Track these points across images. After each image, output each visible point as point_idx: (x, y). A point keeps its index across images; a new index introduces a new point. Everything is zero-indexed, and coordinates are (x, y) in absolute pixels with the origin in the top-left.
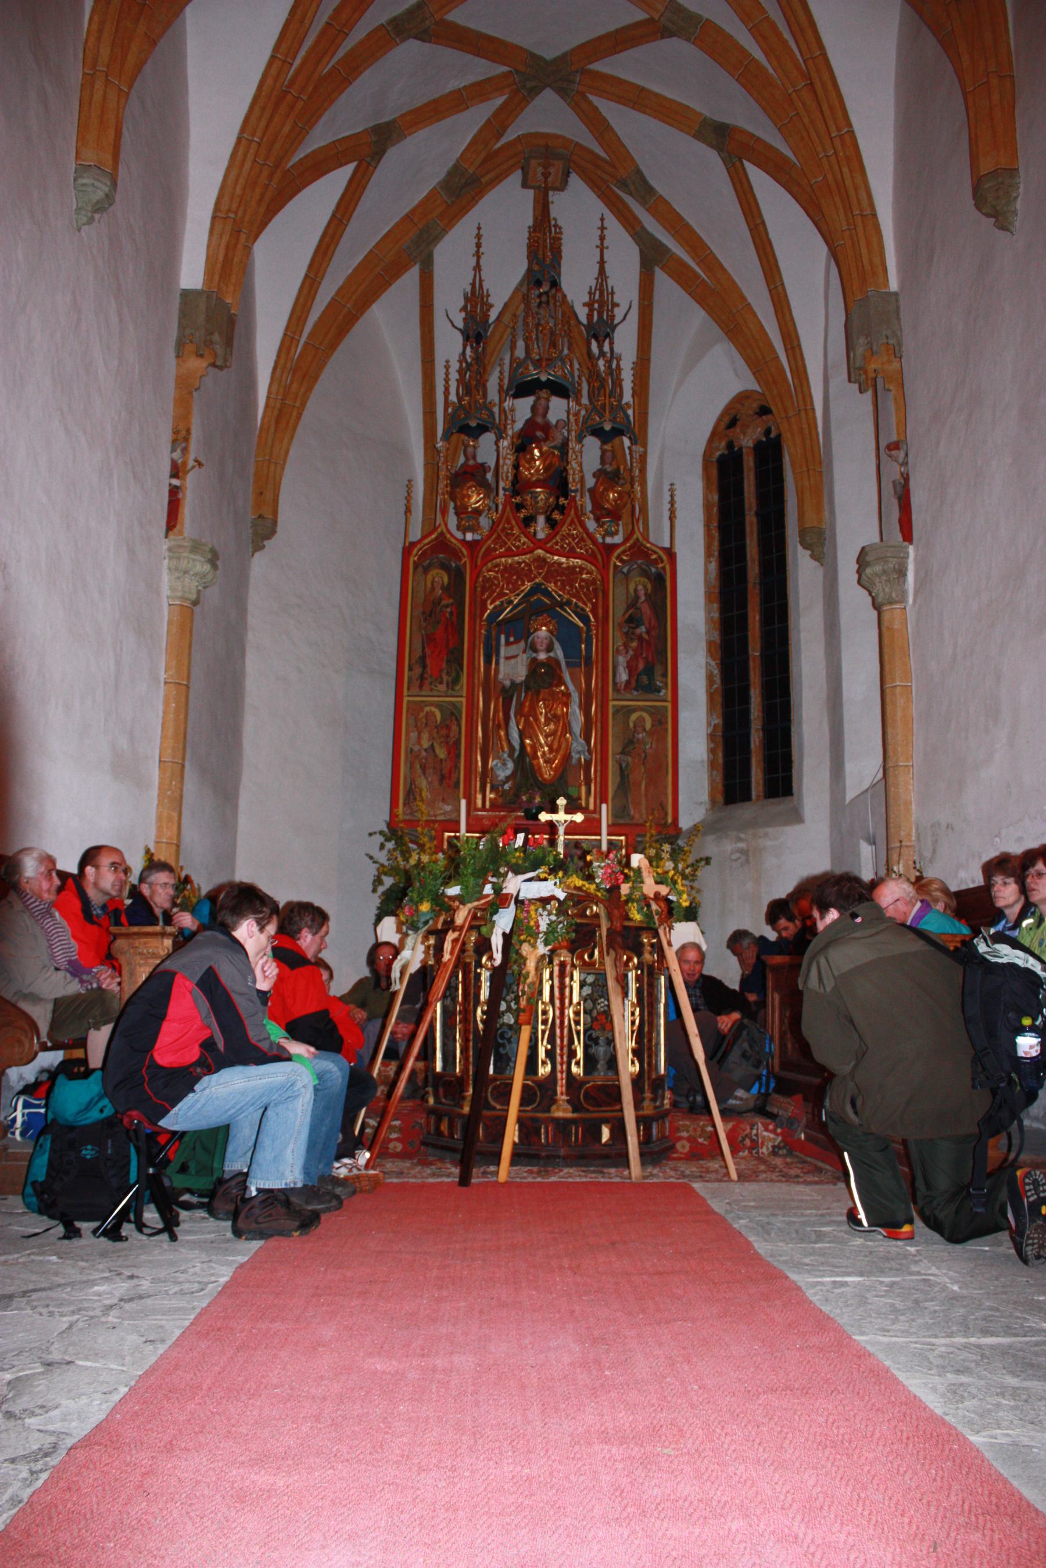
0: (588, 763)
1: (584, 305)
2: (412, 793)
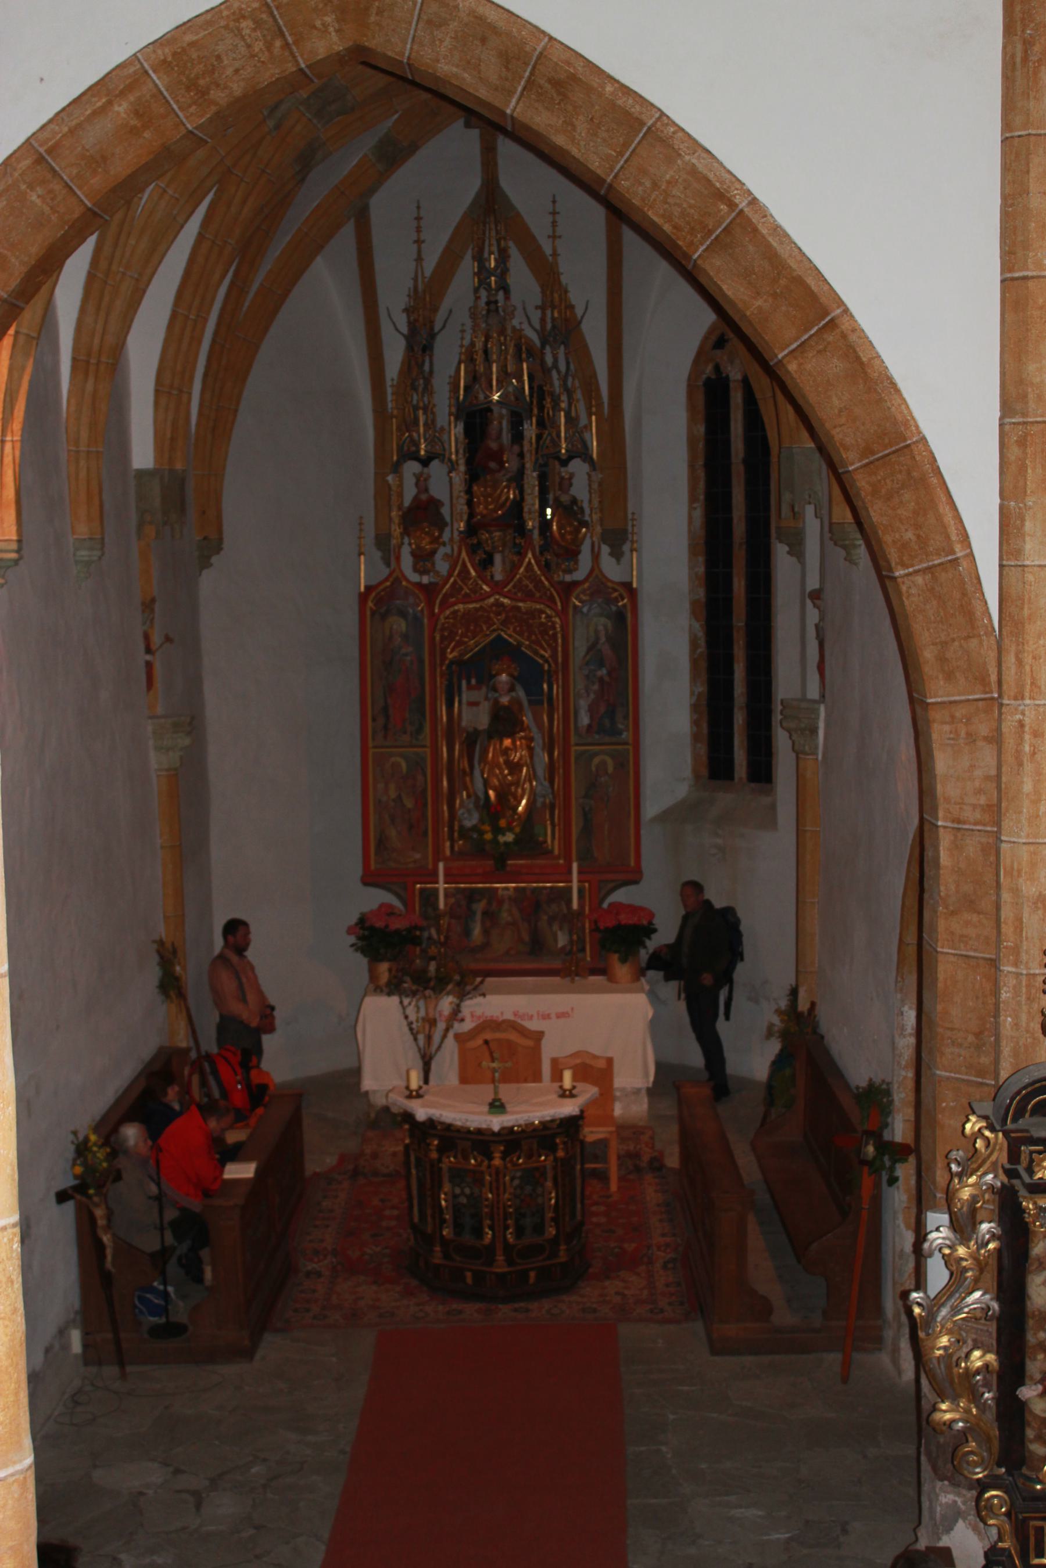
0: (552, 807)
1: (537, 308)
2: (382, 842)
